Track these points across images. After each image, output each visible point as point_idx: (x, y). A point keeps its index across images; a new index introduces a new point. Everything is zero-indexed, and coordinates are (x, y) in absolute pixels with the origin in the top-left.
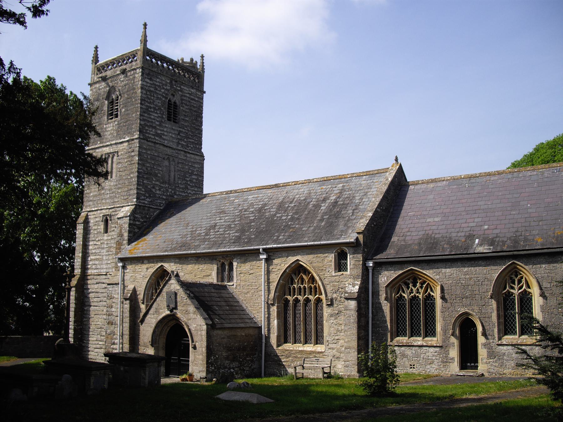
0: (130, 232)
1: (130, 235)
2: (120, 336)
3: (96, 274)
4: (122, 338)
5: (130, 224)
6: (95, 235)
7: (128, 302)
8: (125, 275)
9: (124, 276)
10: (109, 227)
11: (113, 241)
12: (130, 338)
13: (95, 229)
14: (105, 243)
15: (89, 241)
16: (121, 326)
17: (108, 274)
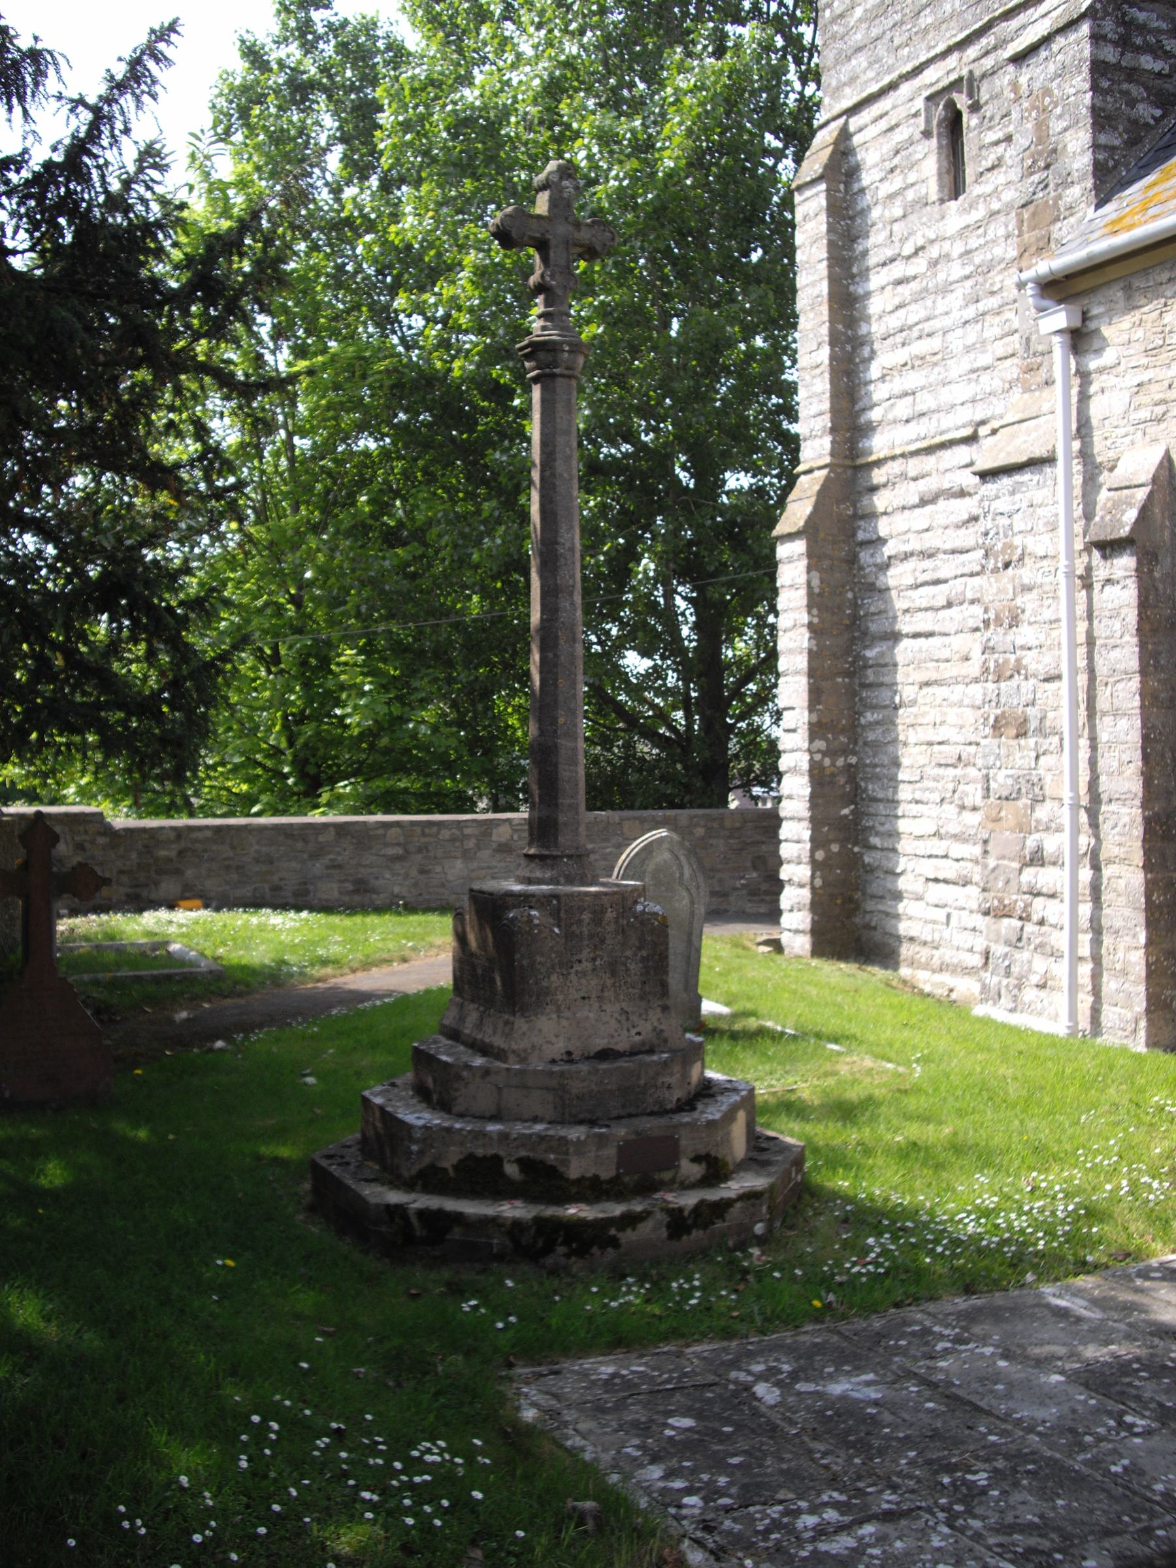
0: (1101, 119)
1: (1103, 139)
2: (1075, 807)
3: (913, 447)
4: (1094, 825)
5: (1098, 68)
6: (896, 227)
7: (1126, 563)
8: (1093, 389)
9: (1084, 397)
10: (969, 150)
11: (997, 229)
12: (1147, 821)
13: (891, 197)
14: (955, 254)
15: (865, 274)
16: (1084, 743)
17: (983, 431)
